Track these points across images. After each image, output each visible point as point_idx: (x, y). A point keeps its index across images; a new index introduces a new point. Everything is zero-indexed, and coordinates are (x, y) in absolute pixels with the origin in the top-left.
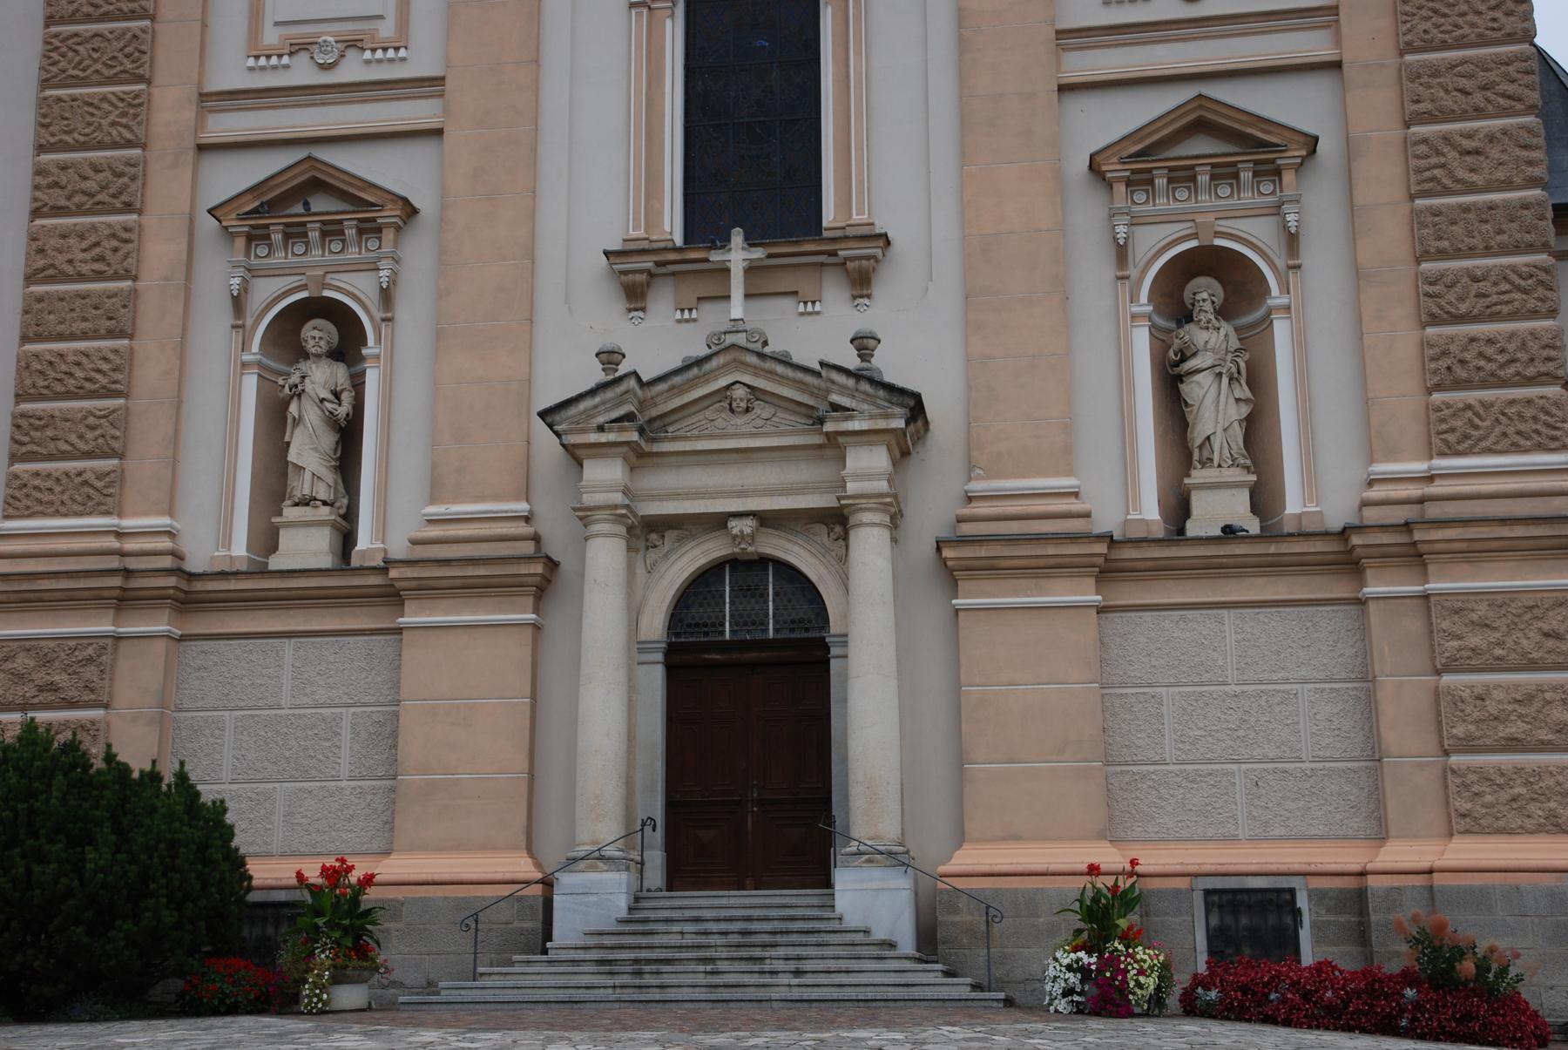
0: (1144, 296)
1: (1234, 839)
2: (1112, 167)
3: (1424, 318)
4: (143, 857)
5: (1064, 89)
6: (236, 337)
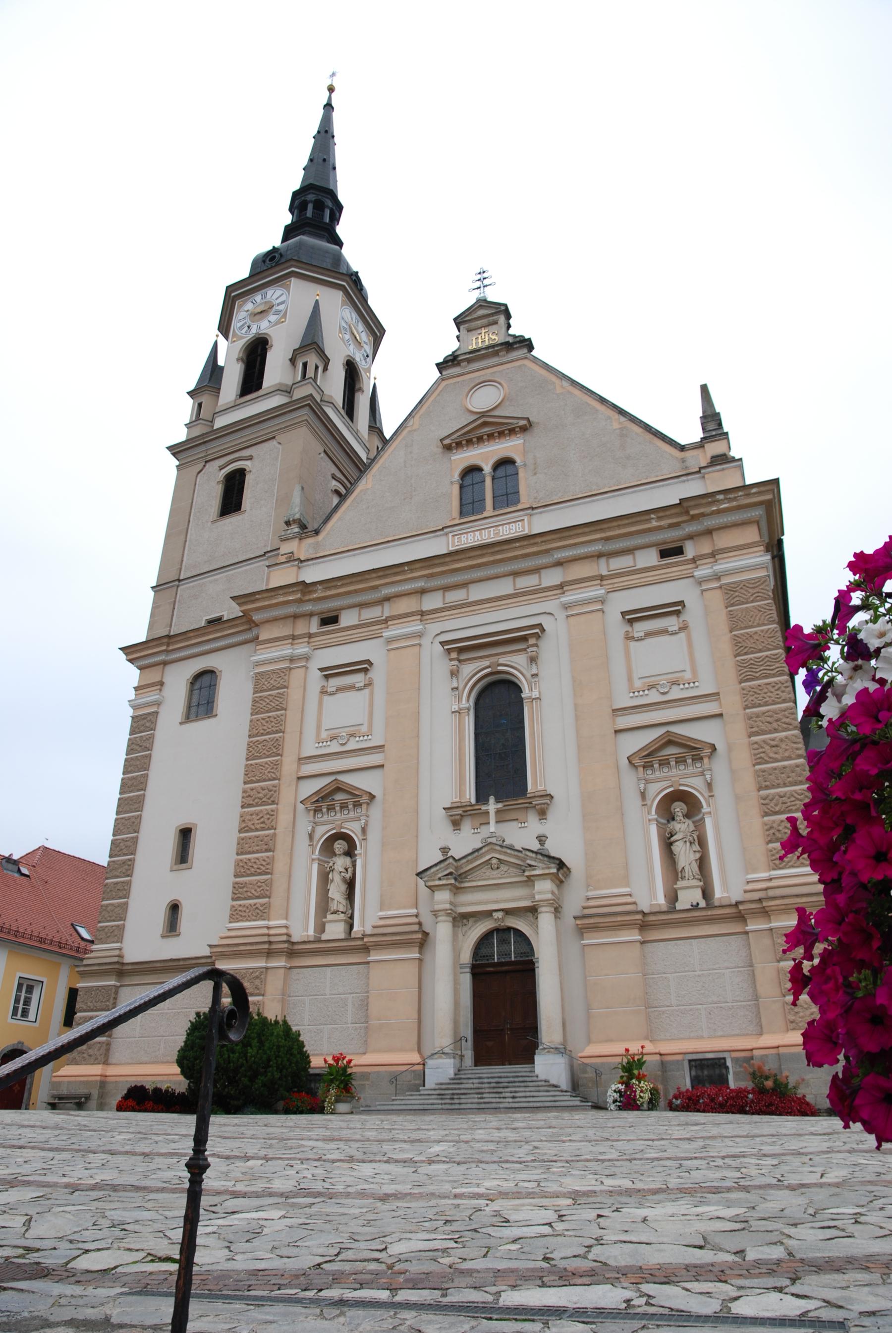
0: (653, 812)
1: (702, 1037)
2: (636, 761)
3: (762, 813)
4: (268, 1052)
5: (617, 732)
6: (310, 849)
